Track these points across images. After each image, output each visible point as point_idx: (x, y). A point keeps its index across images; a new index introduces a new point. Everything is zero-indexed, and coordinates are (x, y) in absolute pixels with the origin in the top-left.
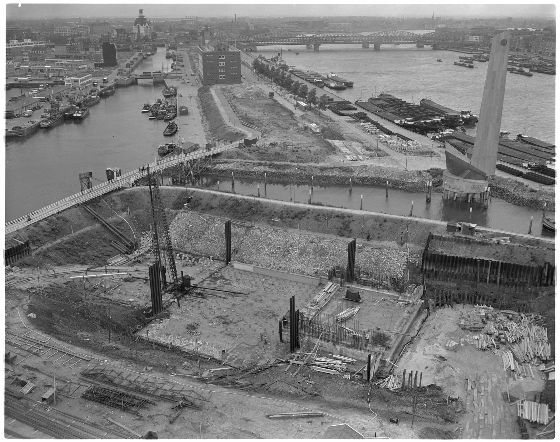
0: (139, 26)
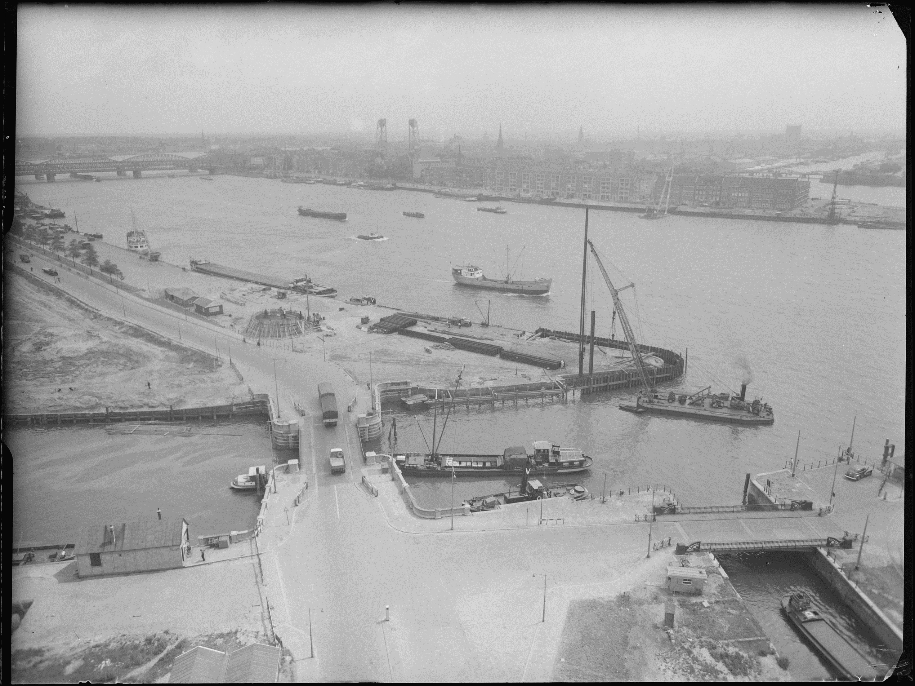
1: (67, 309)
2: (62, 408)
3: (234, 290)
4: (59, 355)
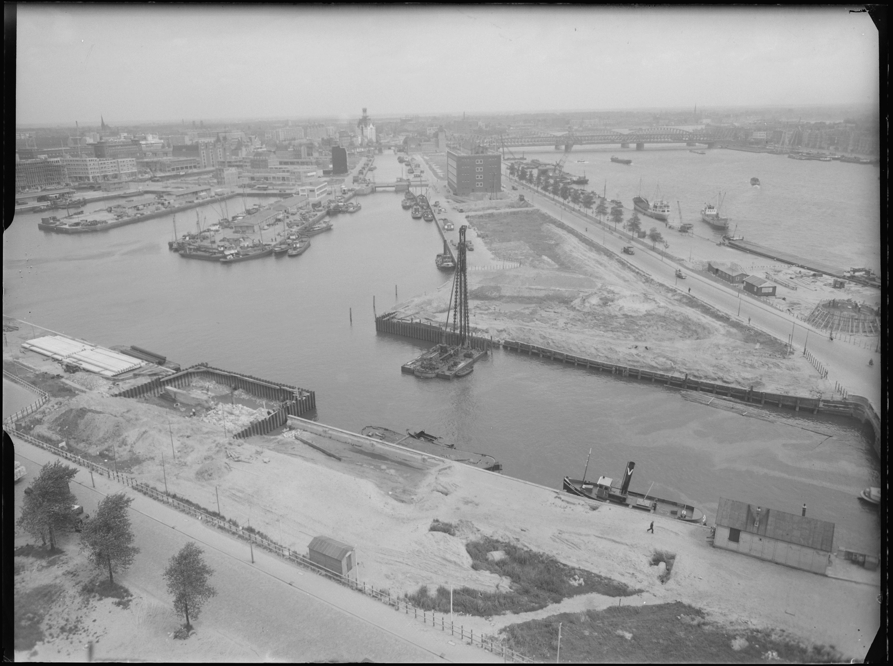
0: (362, 127)
1: (620, 269)
2: (639, 364)
3: (779, 271)
4: (622, 312)
